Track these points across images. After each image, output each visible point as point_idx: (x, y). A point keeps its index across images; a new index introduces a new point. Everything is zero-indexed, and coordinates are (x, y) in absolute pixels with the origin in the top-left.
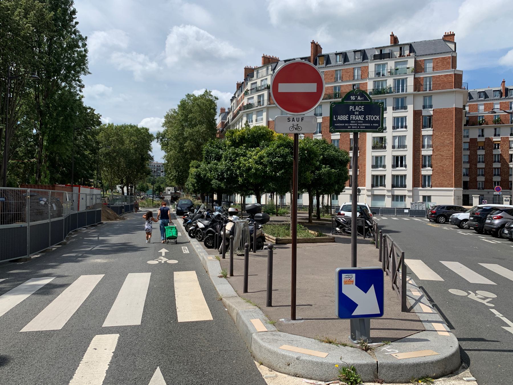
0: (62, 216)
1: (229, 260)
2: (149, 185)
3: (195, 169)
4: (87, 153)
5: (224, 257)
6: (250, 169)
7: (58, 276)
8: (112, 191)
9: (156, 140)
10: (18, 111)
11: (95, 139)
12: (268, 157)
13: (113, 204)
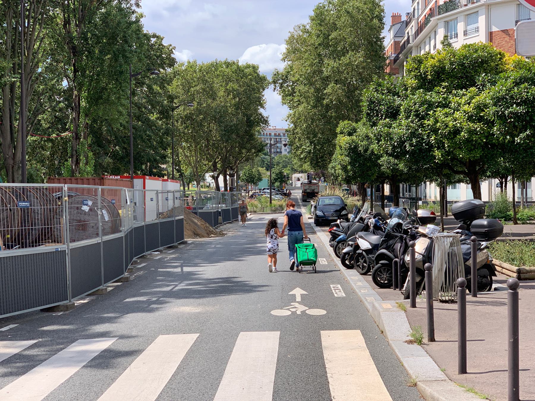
0: (121, 231)
1: (425, 312)
2: (262, 170)
3: (347, 138)
4: (153, 117)
5: (414, 305)
6: (457, 131)
7: (122, 337)
8: (198, 184)
9: (272, 86)
10: (38, 48)
11: (166, 92)
12: (495, 105)
13: (202, 208)
